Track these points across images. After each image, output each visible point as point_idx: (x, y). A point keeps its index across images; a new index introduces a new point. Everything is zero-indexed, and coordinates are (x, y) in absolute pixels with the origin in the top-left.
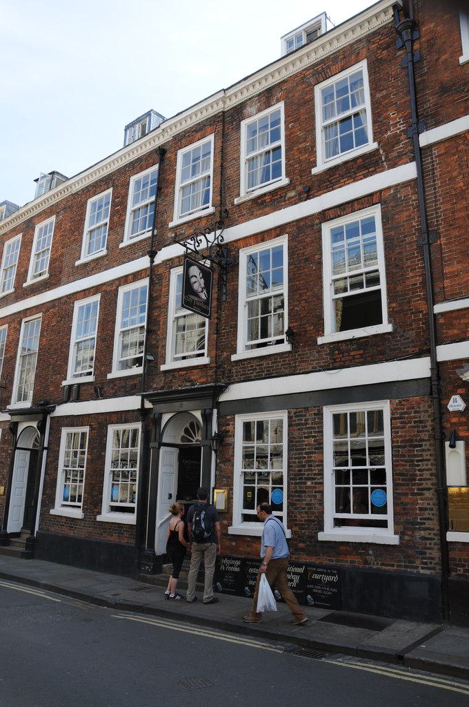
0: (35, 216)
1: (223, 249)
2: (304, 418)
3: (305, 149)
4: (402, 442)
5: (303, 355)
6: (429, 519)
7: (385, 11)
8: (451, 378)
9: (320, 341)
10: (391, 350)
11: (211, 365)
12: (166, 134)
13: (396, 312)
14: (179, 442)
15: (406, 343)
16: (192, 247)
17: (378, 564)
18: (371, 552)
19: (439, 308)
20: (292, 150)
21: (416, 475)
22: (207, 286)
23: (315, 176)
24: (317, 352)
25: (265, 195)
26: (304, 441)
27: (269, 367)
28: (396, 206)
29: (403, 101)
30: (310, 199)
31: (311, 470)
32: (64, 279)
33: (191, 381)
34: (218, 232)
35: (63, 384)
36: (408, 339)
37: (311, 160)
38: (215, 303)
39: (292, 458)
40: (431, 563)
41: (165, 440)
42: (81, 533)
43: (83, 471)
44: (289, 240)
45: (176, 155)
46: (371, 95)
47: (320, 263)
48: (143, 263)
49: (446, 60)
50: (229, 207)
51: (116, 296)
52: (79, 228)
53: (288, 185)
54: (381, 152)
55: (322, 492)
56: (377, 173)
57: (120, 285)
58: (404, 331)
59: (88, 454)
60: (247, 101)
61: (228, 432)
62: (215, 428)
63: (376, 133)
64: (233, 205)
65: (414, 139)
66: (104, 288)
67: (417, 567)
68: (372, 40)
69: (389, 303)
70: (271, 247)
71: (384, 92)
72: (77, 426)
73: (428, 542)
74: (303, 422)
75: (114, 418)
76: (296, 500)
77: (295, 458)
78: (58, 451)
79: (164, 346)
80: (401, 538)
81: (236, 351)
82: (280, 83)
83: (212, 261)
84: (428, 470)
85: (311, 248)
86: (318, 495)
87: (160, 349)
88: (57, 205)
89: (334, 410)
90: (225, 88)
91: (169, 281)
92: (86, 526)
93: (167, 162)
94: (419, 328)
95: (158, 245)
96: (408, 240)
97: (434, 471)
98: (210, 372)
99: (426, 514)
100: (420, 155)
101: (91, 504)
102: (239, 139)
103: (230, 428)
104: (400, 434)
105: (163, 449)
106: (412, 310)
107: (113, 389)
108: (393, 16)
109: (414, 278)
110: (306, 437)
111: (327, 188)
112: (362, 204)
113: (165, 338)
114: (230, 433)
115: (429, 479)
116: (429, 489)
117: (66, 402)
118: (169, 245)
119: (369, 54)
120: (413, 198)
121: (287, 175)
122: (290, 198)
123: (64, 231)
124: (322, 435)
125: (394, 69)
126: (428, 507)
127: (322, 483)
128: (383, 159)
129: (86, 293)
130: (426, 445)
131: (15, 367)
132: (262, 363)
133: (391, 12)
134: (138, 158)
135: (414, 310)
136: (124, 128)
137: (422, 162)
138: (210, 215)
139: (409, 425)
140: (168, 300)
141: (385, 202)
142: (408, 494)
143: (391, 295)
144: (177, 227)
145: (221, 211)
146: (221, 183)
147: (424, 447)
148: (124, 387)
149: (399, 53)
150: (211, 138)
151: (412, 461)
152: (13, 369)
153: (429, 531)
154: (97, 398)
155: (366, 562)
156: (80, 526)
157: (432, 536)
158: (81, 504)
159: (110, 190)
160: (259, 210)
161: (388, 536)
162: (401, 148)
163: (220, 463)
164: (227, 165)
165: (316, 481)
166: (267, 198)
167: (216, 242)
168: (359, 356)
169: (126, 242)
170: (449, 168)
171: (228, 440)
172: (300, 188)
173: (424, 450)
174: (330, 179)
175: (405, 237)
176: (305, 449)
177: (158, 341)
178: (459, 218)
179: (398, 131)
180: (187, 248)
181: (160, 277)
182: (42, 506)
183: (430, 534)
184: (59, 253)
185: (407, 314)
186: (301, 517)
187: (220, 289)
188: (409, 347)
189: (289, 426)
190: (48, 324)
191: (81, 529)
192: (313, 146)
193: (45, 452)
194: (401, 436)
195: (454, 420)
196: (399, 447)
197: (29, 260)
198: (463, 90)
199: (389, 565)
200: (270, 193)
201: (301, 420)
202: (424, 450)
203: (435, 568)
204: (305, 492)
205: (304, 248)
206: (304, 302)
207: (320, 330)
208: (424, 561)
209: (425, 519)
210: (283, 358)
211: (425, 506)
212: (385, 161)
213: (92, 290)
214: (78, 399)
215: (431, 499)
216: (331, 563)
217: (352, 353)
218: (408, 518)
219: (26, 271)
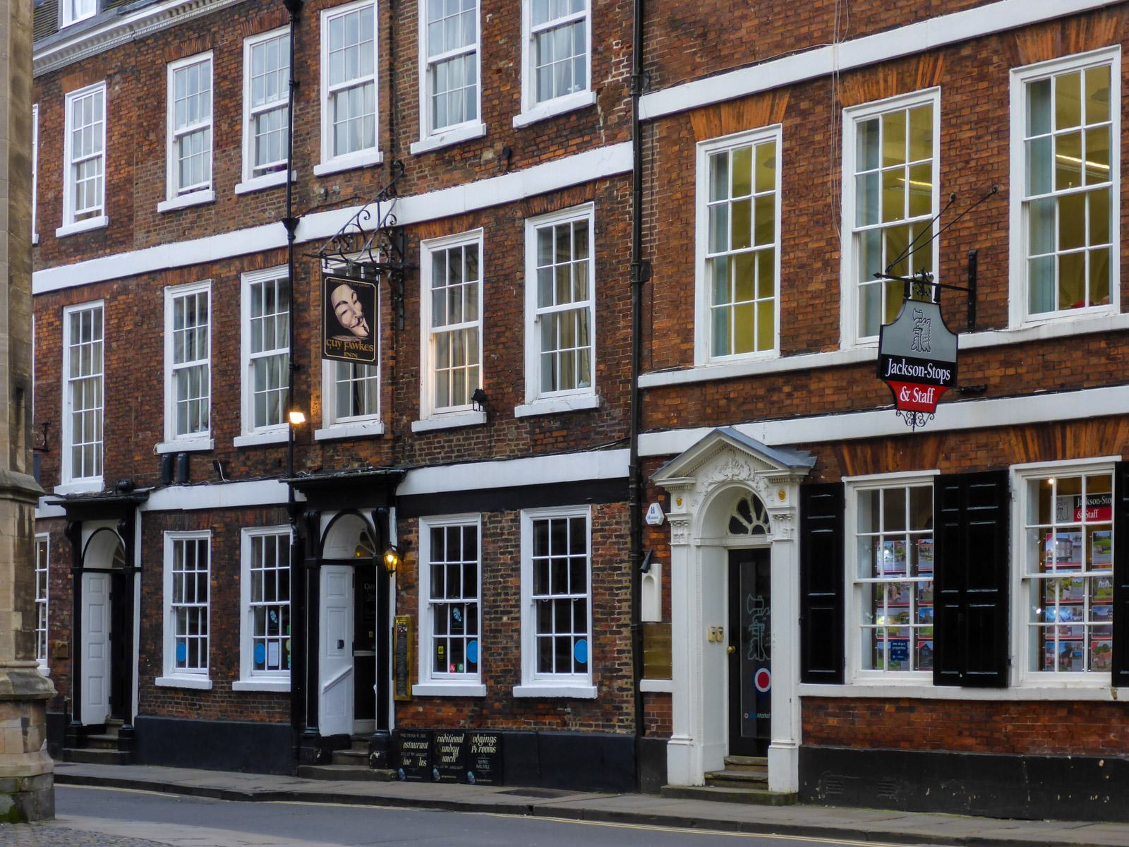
2: (500, 525)
17: (576, 725)
18: (569, 710)
19: (646, 380)
21: (614, 607)
22: (368, 313)
23: (520, 129)
26: (500, 559)
27: (460, 445)
31: (507, 600)
32: (140, 235)
40: (627, 720)
41: (327, 555)
42: (209, 714)
47: (521, 287)
48: (273, 235)
50: (403, 157)
54: (599, 109)
57: (242, 270)
59: (212, 579)
66: (216, 269)
67: (613, 726)
69: (598, 363)
72: (190, 528)
73: (625, 693)
74: (498, 531)
76: (492, 643)
77: (490, 583)
78: (161, 574)
80: (599, 690)
100: (640, 130)
101: (222, 664)
103: (412, 537)
104: (600, 552)
105: (325, 570)
110: (502, 553)
114: (413, 546)
121: (484, 119)
123: (128, 125)
126: (626, 648)
129: (184, 273)
132: (451, 437)
141: (600, 200)
147: (624, 571)
153: (625, 680)
154: (218, 481)
163: (402, 590)
168: (562, 439)
175: (619, 262)
176: (499, 570)
177: (309, 387)
182: (141, 673)
183: (627, 683)
184: (123, 174)
188: (615, 431)
190: (119, 326)
191: (210, 706)
192: (518, 71)
193: (138, 577)
194: (601, 555)
195: (654, 536)
204: (500, 631)
211: (623, 647)
212: (603, 128)
213: (194, 270)
216: (529, 727)
217: (555, 434)
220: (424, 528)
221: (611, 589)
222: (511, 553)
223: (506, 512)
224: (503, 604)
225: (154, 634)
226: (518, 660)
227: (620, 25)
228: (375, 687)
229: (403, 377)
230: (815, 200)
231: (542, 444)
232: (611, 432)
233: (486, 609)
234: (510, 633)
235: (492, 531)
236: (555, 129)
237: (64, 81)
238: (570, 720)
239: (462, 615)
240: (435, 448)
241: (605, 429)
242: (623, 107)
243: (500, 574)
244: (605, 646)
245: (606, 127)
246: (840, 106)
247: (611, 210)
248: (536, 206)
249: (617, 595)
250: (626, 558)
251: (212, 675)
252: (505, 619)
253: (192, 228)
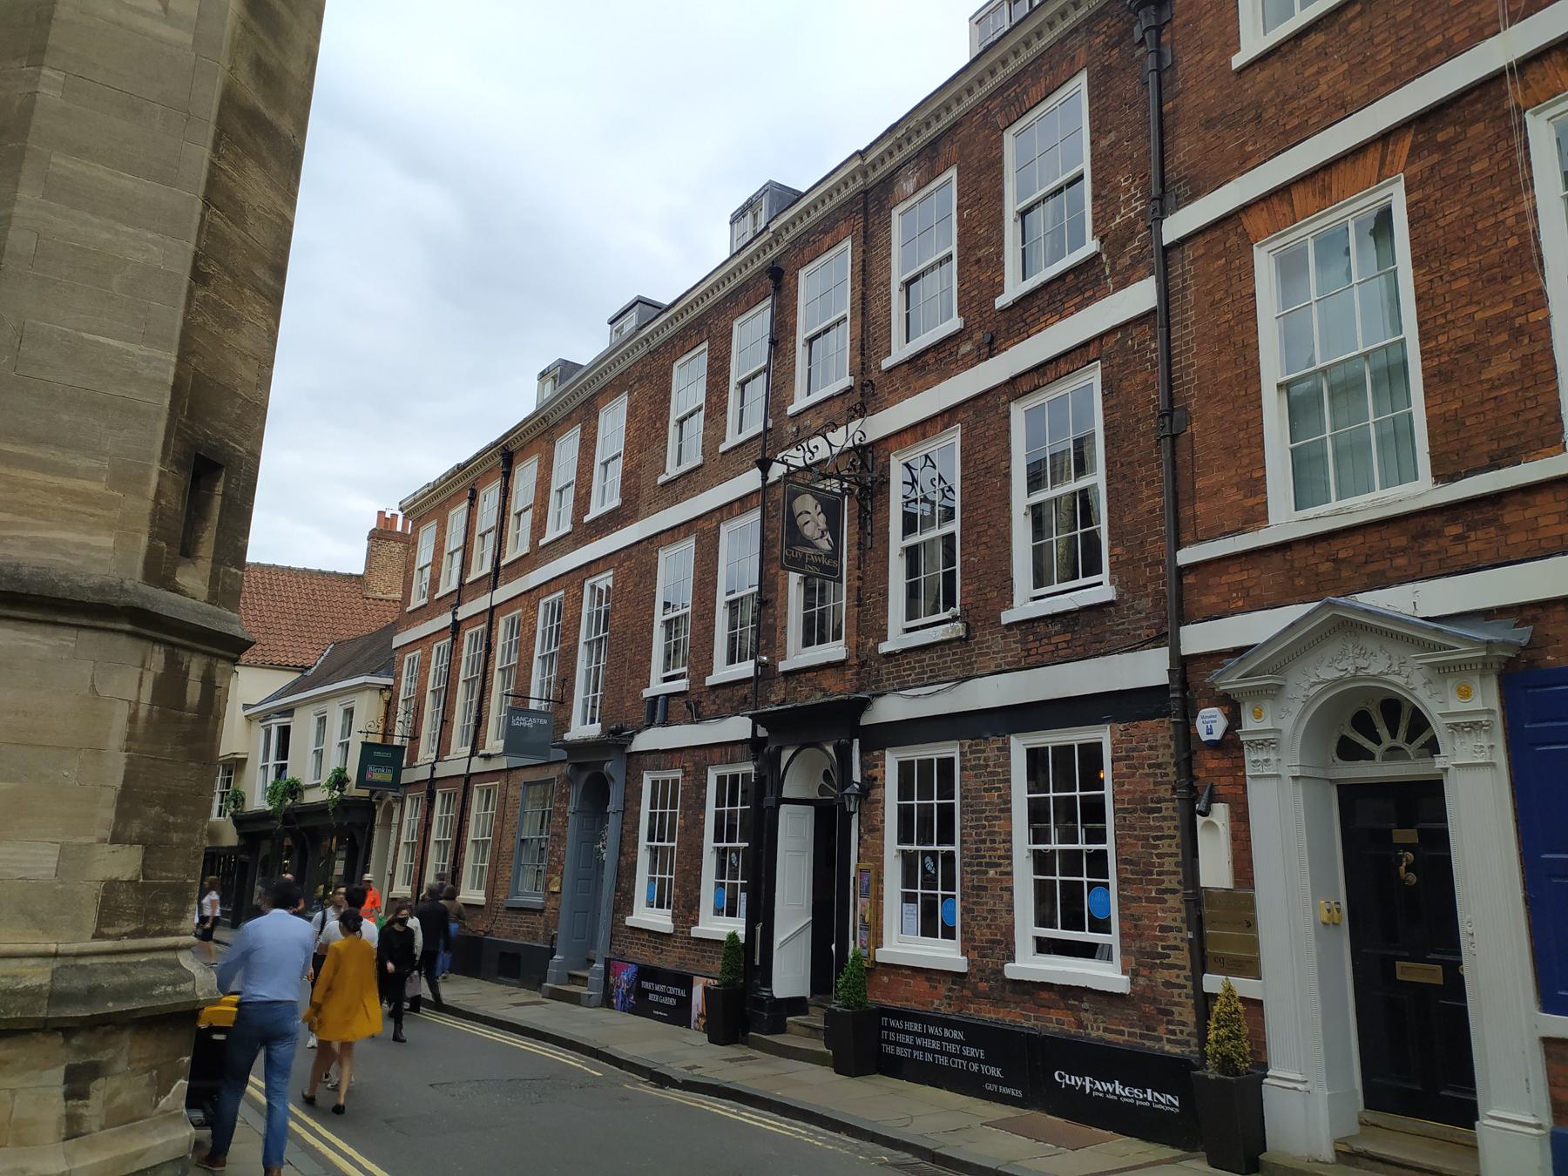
1: (1426, 11)
3: (988, 259)
5: (983, 643)
6: (1176, 948)
9: (1007, 617)
17: (1098, 1029)
21: (1153, 864)
22: (834, 527)
27: (933, 665)
31: (995, 850)
32: (643, 508)
33: (822, 690)
40: (1182, 1032)
46: (1092, 143)
48: (750, 481)
50: (874, 376)
53: (961, 331)
54: (1104, 257)
56: (1096, 300)
61: (876, 779)
62: (857, 777)
67: (1161, 1039)
69: (1111, 548)
73: (1176, 991)
76: (974, 903)
77: (971, 827)
80: (1132, 982)
84: (1171, 855)
86: (1006, 895)
89: (1032, 741)
90: (862, 148)
96: (1142, 428)
97: (1180, 859)
98: (849, 674)
99: (1173, 938)
109: (1154, 499)
110: (986, 790)
114: (878, 782)
116: (1173, 891)
117: (649, 726)
119: (1090, 58)
126: (1174, 924)
127: (1010, 874)
137: (1166, 274)
146: (863, 331)
147: (1164, 813)
148: (729, 699)
152: (574, 669)
155: (1080, 1024)
156: (669, 946)
160: (919, 378)
161: (1107, 975)
164: (872, 294)
168: (1065, 645)
172: (978, 336)
173: (1164, 819)
174: (1025, 317)
176: (983, 811)
179: (1132, 214)
180: (789, 465)
185: (1139, 567)
186: (983, 935)
188: (1141, 628)
194: (1128, 792)
202: (1164, 819)
203: (1188, 1041)
204: (985, 889)
207: (1007, 600)
215: (1179, 911)
219: (589, 494)
220: (891, 761)
221: (1146, 838)
222: (998, 789)
223: (991, 739)
225: (626, 873)
226: (1011, 928)
227: (1131, 157)
229: (870, 597)
230: (1482, 250)
231: (1037, 654)
232: (1135, 629)
234: (999, 892)
235: (973, 763)
236: (1047, 297)
238: (1088, 1019)
239: (936, 866)
241: (1125, 626)
242: (1136, 244)
244: (1139, 919)
245: (1113, 273)
246: (1520, 111)
247: (1124, 364)
249: (1156, 847)
250: (1168, 795)
251: (675, 918)
252: (992, 873)
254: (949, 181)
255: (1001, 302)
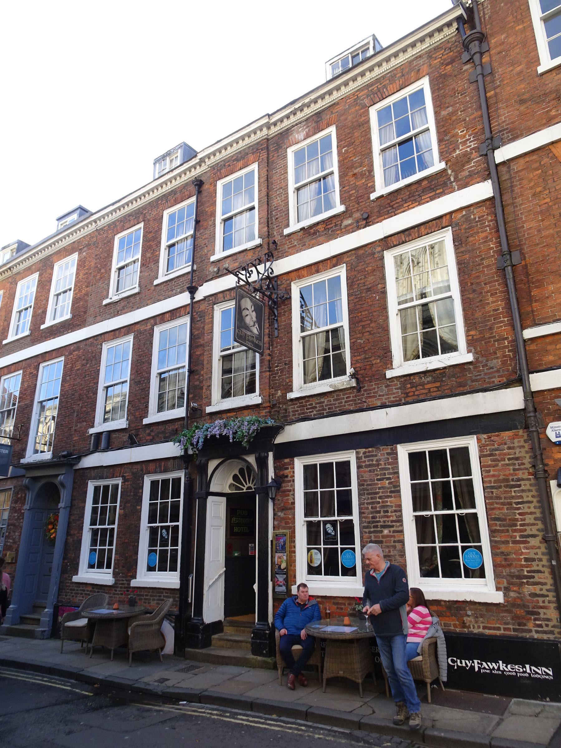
0: (53, 254)
2: (375, 459)
3: (362, 175)
4: (495, 482)
5: (370, 390)
6: (539, 571)
7: (449, 25)
8: (549, 409)
9: (389, 374)
10: (473, 381)
11: (264, 405)
12: (203, 164)
13: (476, 340)
14: (227, 490)
15: (489, 374)
16: (243, 277)
17: (479, 627)
19: (529, 333)
20: (347, 175)
21: (517, 520)
22: (259, 320)
24: (386, 387)
25: (318, 224)
26: (377, 484)
27: (330, 405)
28: (470, 228)
29: (473, 117)
30: (369, 226)
32: (90, 319)
34: (268, 264)
35: (90, 433)
36: (492, 368)
37: (369, 185)
38: (266, 339)
39: (364, 504)
40: (547, 625)
43: (113, 529)
44: (347, 270)
45: (215, 186)
47: (384, 293)
48: (184, 299)
49: (521, 72)
50: (277, 238)
51: (152, 335)
52: (106, 265)
54: (449, 172)
55: (402, 542)
56: (445, 194)
58: (487, 361)
59: (120, 509)
60: (293, 126)
61: (287, 476)
62: (271, 473)
63: (443, 152)
64: (282, 235)
65: (487, 156)
67: (530, 631)
68: (434, 56)
70: (326, 278)
71: (450, 109)
73: (541, 599)
74: (374, 462)
75: (152, 466)
77: (368, 504)
79: (210, 386)
80: (505, 595)
81: (292, 388)
82: (330, 106)
83: (263, 294)
84: (531, 513)
85: (372, 277)
87: (204, 390)
88: (79, 241)
90: (270, 113)
91: (213, 318)
92: (118, 594)
93: (205, 194)
94: (505, 356)
95: (199, 281)
96: (485, 263)
97: (538, 515)
102: (286, 167)
105: (210, 499)
106: (495, 336)
107: (149, 435)
108: (457, 29)
111: (388, 213)
112: (430, 228)
113: (210, 378)
114: (289, 479)
115: (533, 524)
116: (534, 536)
118: (211, 279)
120: (490, 218)
121: (342, 202)
122: (346, 226)
123: (89, 269)
124: (398, 477)
125: (461, 84)
126: (536, 557)
127: (402, 531)
128: (452, 179)
130: (525, 485)
131: (31, 416)
132: (322, 400)
133: (455, 25)
134: (172, 191)
135: (497, 338)
136: (153, 162)
138: (257, 247)
139: (503, 463)
140: (212, 338)
141: (457, 224)
142: (508, 541)
143: (469, 322)
144: (219, 261)
145: (269, 243)
146: (268, 214)
147: (523, 487)
149: (465, 68)
150: (255, 167)
151: (510, 504)
155: (464, 625)
157: (544, 592)
158: (111, 571)
159: (141, 225)
162: (471, 167)
164: (273, 194)
165: (395, 529)
166: (321, 227)
167: (266, 274)
168: (435, 389)
169: (161, 279)
170: (532, 184)
171: (286, 486)
172: (357, 215)
173: (523, 491)
174: (392, 204)
177: (201, 382)
178: (547, 237)
179: (468, 149)
180: (239, 278)
181: (203, 315)
183: (541, 590)
185: (490, 342)
187: (271, 324)
188: (495, 377)
189: (359, 467)
192: (371, 170)
194: (493, 476)
196: (492, 487)
197: (47, 301)
198: (543, 101)
199: (494, 629)
200: (323, 221)
201: (372, 460)
202: (523, 491)
205: (365, 277)
206: (368, 333)
208: (537, 622)
209: (534, 571)
210: (346, 394)
211: (532, 556)
214: (108, 448)
218: (512, 571)
224: (382, 520)
228: (256, 587)
229: (277, 366)
233: (365, 524)
237: (55, 258)
239: (168, 534)
240: (307, 409)
243: (378, 495)
248: (395, 240)
251: (115, 575)
253: (124, 309)
254: (140, 228)
255: (373, 196)
